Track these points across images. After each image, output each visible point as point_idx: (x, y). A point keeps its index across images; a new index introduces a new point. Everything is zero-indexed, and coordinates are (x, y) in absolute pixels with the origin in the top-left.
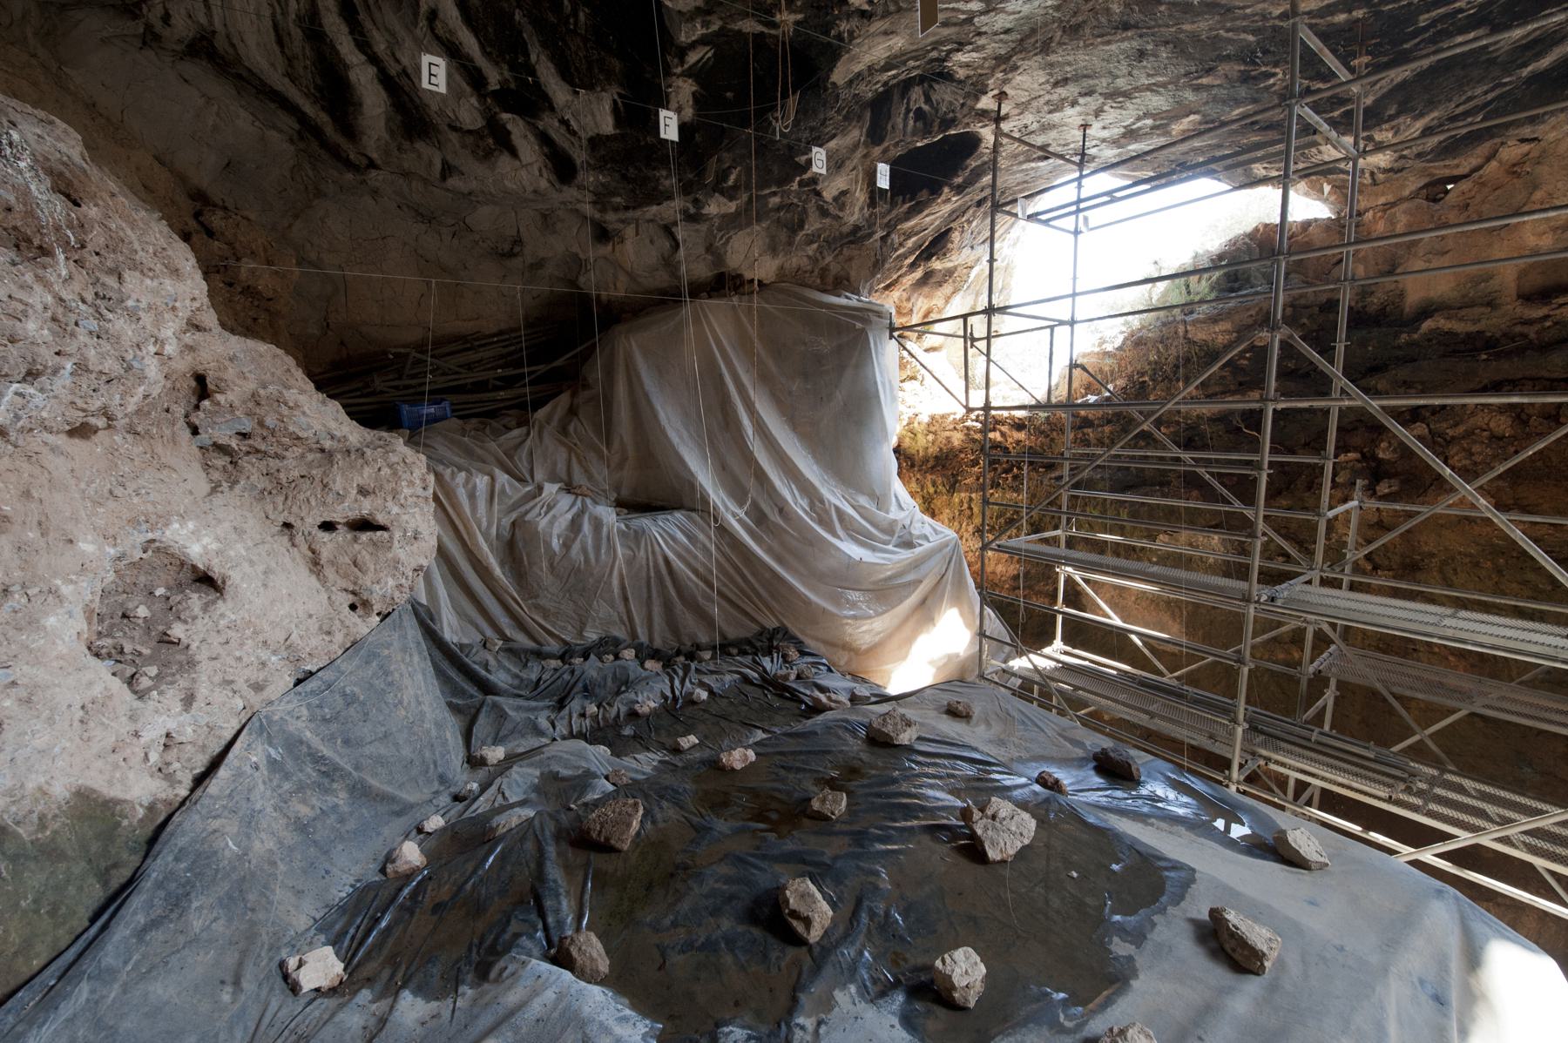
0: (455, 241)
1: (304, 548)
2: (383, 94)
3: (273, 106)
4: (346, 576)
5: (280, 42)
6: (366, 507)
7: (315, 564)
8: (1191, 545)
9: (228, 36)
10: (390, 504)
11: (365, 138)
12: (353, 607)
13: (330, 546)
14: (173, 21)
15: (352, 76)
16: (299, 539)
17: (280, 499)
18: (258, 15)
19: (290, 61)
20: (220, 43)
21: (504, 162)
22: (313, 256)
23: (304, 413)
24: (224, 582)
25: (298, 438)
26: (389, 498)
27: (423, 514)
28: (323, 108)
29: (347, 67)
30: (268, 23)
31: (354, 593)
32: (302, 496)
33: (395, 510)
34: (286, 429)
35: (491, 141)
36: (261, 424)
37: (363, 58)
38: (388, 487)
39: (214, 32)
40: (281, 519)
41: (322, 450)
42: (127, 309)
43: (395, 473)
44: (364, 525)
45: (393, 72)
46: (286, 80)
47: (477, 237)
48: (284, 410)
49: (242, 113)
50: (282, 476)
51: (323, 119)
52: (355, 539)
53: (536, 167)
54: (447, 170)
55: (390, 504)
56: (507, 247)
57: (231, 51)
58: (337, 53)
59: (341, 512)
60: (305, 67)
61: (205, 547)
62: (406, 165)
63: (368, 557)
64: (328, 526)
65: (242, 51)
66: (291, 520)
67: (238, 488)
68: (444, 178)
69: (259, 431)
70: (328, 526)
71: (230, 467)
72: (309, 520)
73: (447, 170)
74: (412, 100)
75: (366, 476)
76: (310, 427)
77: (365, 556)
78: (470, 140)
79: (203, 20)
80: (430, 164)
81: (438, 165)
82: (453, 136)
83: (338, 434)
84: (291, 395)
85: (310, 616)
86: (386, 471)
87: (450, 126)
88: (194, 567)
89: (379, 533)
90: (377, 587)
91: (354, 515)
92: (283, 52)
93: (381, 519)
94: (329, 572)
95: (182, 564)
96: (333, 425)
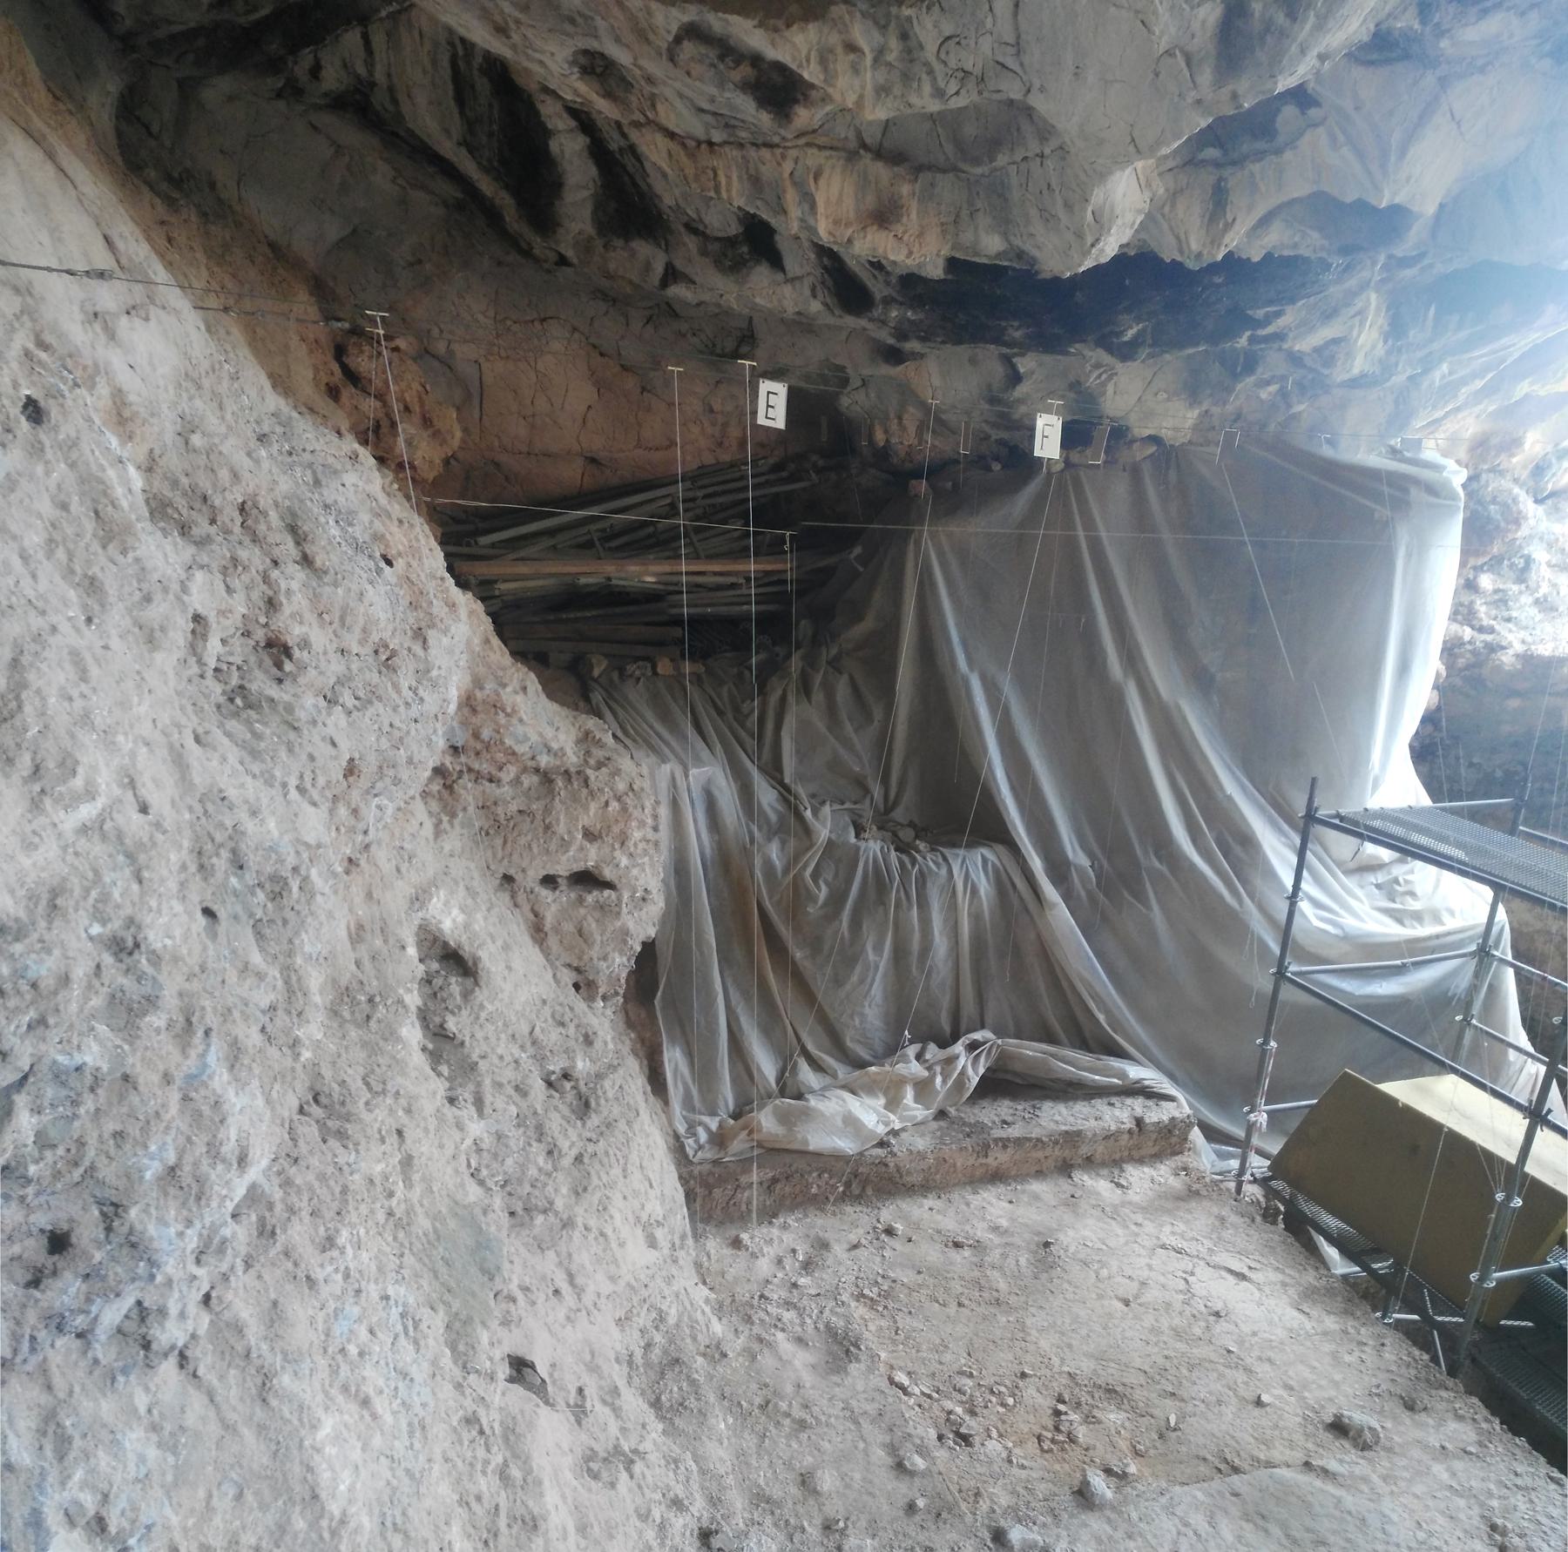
0: (650, 328)
1: (526, 908)
2: (593, 171)
3: (431, 170)
4: (570, 948)
5: (460, 100)
6: (591, 857)
7: (538, 931)
8: (565, 1539)
9: (391, 89)
10: (617, 854)
11: (561, 231)
12: (576, 986)
13: (554, 908)
14: (324, 73)
15: (554, 146)
16: (521, 897)
17: (499, 842)
18: (434, 62)
19: (470, 125)
20: (379, 99)
21: (761, 276)
22: (441, 348)
23: (521, 720)
24: (475, 964)
25: (514, 753)
26: (617, 846)
27: (652, 865)
28: (507, 187)
29: (547, 133)
30: (446, 72)
31: (578, 970)
32: (523, 841)
33: (624, 861)
34: (502, 743)
35: (745, 249)
36: (476, 735)
37: (573, 123)
38: (616, 830)
39: (373, 85)
40: (502, 871)
41: (537, 770)
42: (431, 679)
43: (624, 809)
44: (586, 879)
45: (613, 146)
46: (463, 151)
47: (684, 327)
48: (502, 718)
49: (383, 167)
50: (500, 810)
51: (505, 201)
52: (581, 900)
53: (807, 282)
54: (672, 275)
55: (617, 854)
56: (730, 345)
57: (391, 108)
58: (537, 114)
59: (563, 866)
60: (491, 135)
61: (454, 921)
62: (612, 266)
63: (594, 925)
64: (549, 881)
65: (406, 109)
66: (512, 872)
67: (456, 822)
68: (664, 283)
69: (472, 742)
70: (549, 881)
71: (446, 794)
72: (531, 873)
73: (672, 275)
74: (635, 184)
75: (590, 816)
76: (527, 739)
77: (591, 925)
78: (716, 247)
79: (361, 70)
80: (648, 267)
81: (659, 268)
82: (691, 243)
83: (555, 746)
84: (509, 696)
85: (544, 1002)
86: (614, 805)
87: (687, 226)
88: (446, 944)
89: (607, 892)
90: (603, 965)
91: (578, 867)
92: (462, 113)
93: (608, 874)
94: (553, 941)
95: (435, 939)
96: (549, 733)
